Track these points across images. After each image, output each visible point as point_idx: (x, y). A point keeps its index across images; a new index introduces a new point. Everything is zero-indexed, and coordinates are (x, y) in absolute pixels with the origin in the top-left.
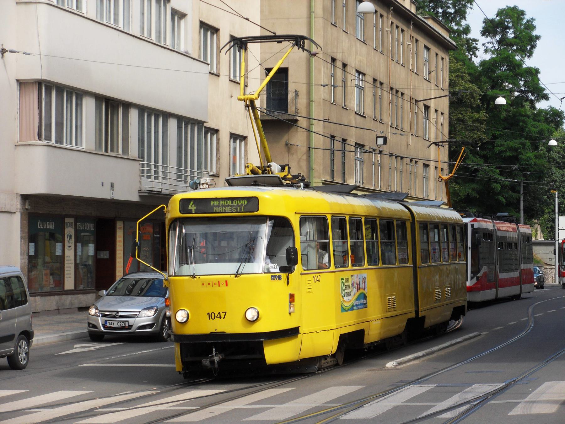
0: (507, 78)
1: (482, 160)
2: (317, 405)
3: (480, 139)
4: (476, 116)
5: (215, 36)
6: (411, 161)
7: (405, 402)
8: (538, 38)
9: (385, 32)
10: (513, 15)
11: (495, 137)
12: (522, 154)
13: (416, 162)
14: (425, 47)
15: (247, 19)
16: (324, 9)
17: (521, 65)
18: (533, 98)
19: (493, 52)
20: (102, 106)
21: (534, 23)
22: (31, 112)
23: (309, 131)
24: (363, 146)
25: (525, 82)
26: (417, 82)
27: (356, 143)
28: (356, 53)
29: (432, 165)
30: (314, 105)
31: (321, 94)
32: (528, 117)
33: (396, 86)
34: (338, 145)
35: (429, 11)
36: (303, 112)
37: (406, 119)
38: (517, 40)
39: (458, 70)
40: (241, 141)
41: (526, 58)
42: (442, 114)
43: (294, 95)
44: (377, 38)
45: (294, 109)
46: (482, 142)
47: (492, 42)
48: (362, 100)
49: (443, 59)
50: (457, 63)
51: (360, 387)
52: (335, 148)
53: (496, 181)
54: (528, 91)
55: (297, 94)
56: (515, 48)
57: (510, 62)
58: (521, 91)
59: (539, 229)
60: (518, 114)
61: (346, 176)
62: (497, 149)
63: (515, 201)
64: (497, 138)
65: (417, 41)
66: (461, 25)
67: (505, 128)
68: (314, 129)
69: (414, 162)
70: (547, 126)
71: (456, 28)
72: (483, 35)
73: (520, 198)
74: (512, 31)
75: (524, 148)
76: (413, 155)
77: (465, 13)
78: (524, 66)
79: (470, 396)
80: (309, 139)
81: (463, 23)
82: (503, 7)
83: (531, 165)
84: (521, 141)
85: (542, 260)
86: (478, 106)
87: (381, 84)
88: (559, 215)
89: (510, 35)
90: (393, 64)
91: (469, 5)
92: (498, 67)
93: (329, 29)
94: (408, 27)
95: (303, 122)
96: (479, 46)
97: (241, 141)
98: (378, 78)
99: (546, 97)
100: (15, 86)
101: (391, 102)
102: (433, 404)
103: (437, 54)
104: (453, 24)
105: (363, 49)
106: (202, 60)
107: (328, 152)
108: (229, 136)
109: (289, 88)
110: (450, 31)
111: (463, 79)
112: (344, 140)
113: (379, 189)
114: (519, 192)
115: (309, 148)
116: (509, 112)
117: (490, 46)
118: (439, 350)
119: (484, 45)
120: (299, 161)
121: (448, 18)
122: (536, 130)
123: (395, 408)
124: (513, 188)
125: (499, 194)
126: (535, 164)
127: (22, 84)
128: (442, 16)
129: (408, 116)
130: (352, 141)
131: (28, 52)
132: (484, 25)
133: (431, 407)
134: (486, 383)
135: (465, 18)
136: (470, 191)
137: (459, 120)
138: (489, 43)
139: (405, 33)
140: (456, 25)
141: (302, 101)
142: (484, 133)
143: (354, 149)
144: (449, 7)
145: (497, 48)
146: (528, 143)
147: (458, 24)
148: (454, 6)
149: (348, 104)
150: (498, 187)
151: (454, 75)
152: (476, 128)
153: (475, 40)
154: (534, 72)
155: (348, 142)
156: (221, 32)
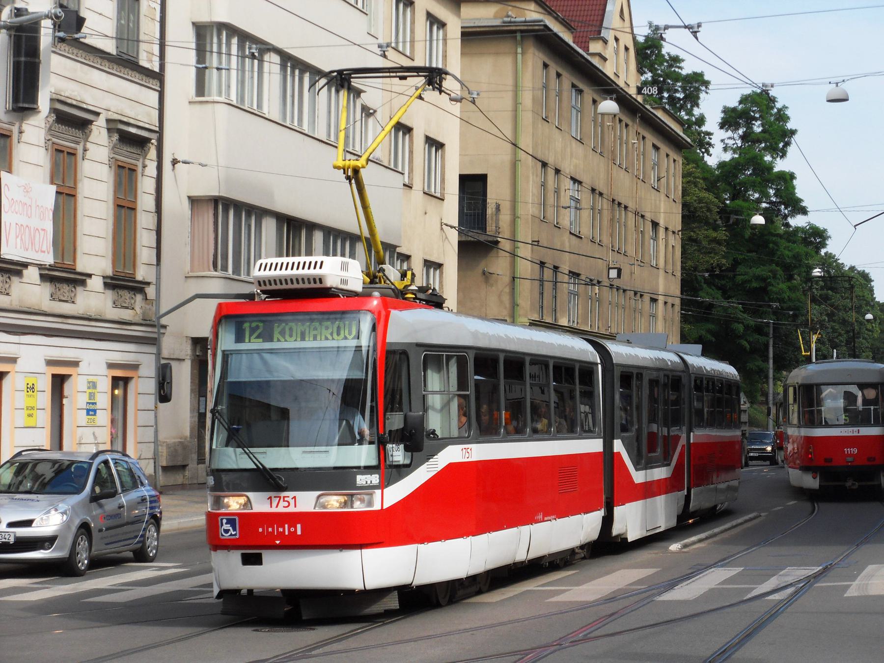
0: (754, 187)
1: (720, 292)
3: (718, 265)
4: (714, 235)
5: (407, 136)
6: (636, 293)
8: (793, 132)
13: (641, 296)
17: (772, 168)
18: (786, 212)
19: (735, 151)
20: (283, 227)
21: (788, 112)
22: (206, 236)
23: (513, 255)
24: (578, 275)
25: (777, 190)
27: (570, 272)
29: (661, 299)
30: (519, 221)
31: (529, 208)
32: (780, 236)
33: (618, 199)
34: (548, 274)
36: (505, 232)
37: (630, 240)
38: (767, 136)
40: (435, 269)
41: (778, 159)
47: (734, 137)
49: (674, 161)
50: (688, 164)
51: (650, 571)
52: (545, 278)
53: (738, 321)
54: (780, 203)
56: (763, 145)
57: (759, 164)
58: (771, 203)
61: (558, 315)
62: (739, 279)
64: (740, 264)
66: (693, 115)
67: (750, 251)
68: (520, 252)
69: (639, 295)
70: (805, 249)
71: (686, 118)
72: (721, 128)
74: (759, 122)
75: (775, 277)
77: (698, 98)
78: (776, 170)
79: (790, 579)
81: (696, 112)
87: (601, 194)
89: (757, 128)
90: (615, 168)
91: (703, 88)
94: (634, 121)
95: (505, 245)
98: (597, 188)
99: (804, 211)
100: (186, 204)
101: (612, 220)
103: (667, 155)
104: (683, 113)
106: (392, 167)
107: (537, 283)
108: (421, 263)
111: (696, 186)
112: (556, 268)
113: (596, 330)
114: (767, 335)
115: (514, 278)
117: (731, 142)
118: (722, 532)
119: (722, 141)
120: (499, 296)
121: (675, 104)
122: (790, 254)
123: (711, 590)
124: (760, 330)
125: (740, 337)
126: (790, 299)
127: (194, 201)
129: (632, 236)
130: (565, 268)
131: (204, 163)
132: (722, 115)
136: (703, 333)
138: (729, 138)
139: (630, 128)
140: (687, 114)
141: (505, 218)
142: (724, 257)
143: (566, 278)
144: (676, 91)
145: (739, 145)
146: (780, 271)
147: (690, 113)
149: (560, 221)
150: (741, 328)
153: (709, 134)
154: (788, 177)
155: (560, 270)
156: (415, 132)
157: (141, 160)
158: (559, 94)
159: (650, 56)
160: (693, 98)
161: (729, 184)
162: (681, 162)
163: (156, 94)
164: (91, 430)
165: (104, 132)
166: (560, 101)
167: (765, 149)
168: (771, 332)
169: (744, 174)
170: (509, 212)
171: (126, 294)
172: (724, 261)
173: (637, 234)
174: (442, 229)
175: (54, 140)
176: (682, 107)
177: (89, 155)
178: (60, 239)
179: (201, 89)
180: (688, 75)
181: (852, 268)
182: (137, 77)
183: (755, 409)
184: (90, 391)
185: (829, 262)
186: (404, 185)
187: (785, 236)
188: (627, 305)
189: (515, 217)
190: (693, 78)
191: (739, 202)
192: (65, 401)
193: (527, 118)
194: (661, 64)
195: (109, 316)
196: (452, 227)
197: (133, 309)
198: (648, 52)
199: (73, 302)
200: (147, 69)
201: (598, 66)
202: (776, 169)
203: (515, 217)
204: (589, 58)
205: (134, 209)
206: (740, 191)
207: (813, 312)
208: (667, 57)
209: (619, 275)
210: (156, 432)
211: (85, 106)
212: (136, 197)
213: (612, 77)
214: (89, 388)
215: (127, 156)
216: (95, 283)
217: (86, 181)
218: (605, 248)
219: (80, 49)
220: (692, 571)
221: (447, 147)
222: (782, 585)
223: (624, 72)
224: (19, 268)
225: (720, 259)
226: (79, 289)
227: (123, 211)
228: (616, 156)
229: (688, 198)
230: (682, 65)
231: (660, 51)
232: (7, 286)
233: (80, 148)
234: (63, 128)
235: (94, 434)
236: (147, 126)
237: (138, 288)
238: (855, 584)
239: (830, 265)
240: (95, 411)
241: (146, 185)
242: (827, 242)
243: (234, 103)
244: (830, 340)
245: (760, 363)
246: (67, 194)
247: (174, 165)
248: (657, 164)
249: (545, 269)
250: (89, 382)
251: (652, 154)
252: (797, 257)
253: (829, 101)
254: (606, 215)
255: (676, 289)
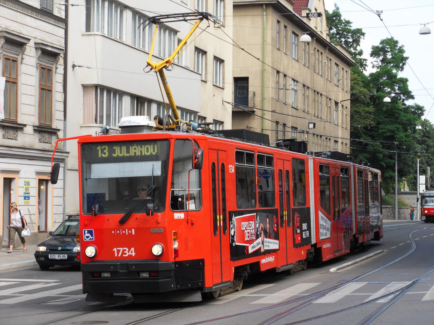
0: (387, 85)
2: (295, 295)
4: (367, 109)
5: (204, 56)
6: (327, 138)
7: (351, 293)
8: (407, 58)
9: (310, 54)
10: (391, 43)
11: (379, 123)
12: (397, 134)
13: (330, 139)
14: (336, 64)
15: (243, 49)
16: (272, 39)
18: (404, 98)
19: (378, 68)
21: (404, 48)
24: (296, 128)
25: (399, 87)
26: (330, 86)
27: (292, 127)
28: (292, 67)
29: (340, 141)
32: (401, 110)
34: (280, 127)
35: (336, 40)
36: (258, 105)
39: (355, 79)
40: (220, 125)
42: (346, 108)
43: (252, 95)
44: (305, 58)
45: (252, 104)
46: (371, 127)
47: (377, 61)
48: (296, 98)
49: (346, 72)
50: (354, 74)
52: (279, 130)
54: (401, 93)
55: (254, 94)
56: (392, 65)
57: (389, 74)
58: (396, 93)
59: (406, 184)
60: (394, 108)
62: (380, 131)
63: (393, 165)
65: (330, 60)
66: (357, 50)
67: (386, 117)
69: (328, 139)
70: (413, 116)
71: (353, 51)
72: (371, 56)
73: (395, 163)
74: (390, 53)
75: (398, 130)
76: (328, 134)
77: (359, 41)
78: (398, 77)
79: (393, 289)
80: (262, 123)
81: (359, 48)
82: (384, 38)
83: (402, 141)
84: (396, 126)
85: (409, 204)
86: (368, 103)
87: (308, 88)
88: (419, 175)
91: (362, 36)
92: (381, 77)
93: (275, 52)
94: (325, 52)
95: (258, 113)
96: (368, 63)
97: (220, 125)
99: (412, 97)
100: (81, 88)
101: (314, 100)
102: (352, 294)
103: (343, 69)
104: (352, 49)
105: (296, 65)
106: (196, 71)
109: (249, 90)
110: (350, 53)
111: (358, 85)
112: (284, 125)
114: (394, 159)
116: (388, 107)
117: (376, 63)
118: (360, 261)
119: (372, 63)
122: (406, 119)
123: (347, 296)
124: (391, 157)
125: (381, 160)
126: (406, 141)
127: (85, 87)
128: (345, 44)
129: (325, 109)
130: (289, 125)
131: (89, 67)
132: (372, 50)
133: (368, 296)
134: (400, 281)
135: (359, 45)
137: (356, 111)
139: (323, 54)
140: (354, 49)
141: (258, 99)
143: (290, 130)
144: (349, 38)
145: (380, 65)
147: (355, 49)
148: (352, 37)
149: (286, 101)
150: (381, 155)
151: (352, 82)
152: (367, 118)
153: (365, 60)
154: (405, 81)
155: (287, 125)
156: (208, 54)
157: (55, 65)
158: (286, 37)
159: (335, 21)
160: (357, 42)
161: (375, 84)
162: (350, 72)
163: (63, 31)
164: (27, 207)
165: (33, 50)
166: (286, 40)
167: (393, 67)
168: (397, 158)
169: (382, 79)
170: (260, 96)
171: (47, 136)
172: (372, 123)
173: (327, 108)
174: (223, 104)
175: (5, 53)
176: (351, 46)
177: (24, 61)
178: (8, 106)
179: (88, 28)
180: (354, 30)
181: (419, 110)
182: (52, 21)
183: (389, 197)
184: (26, 186)
185: (425, 124)
186: (201, 81)
187: (403, 110)
188: (322, 144)
189: (263, 99)
190: (357, 31)
191: (380, 93)
192: (12, 192)
193: (269, 48)
194: (341, 25)
195: (36, 147)
196: (228, 103)
197: (50, 143)
198: (333, 19)
199: (16, 140)
200: (58, 17)
201: (306, 23)
202: (398, 77)
203: (263, 99)
204: (301, 18)
205: (51, 91)
206: (380, 88)
207: (418, 148)
208: (344, 21)
209: (314, 127)
210: (64, 208)
211: (22, 36)
212: (52, 84)
213: (314, 28)
214: (25, 185)
215: (46, 63)
216: (29, 130)
217: (23, 75)
218: (310, 115)
219: (19, 5)
220: (338, 284)
221: (225, 62)
222: (387, 293)
223: (319, 26)
224: (22, 127)
225: (370, 122)
226: (19, 133)
227: (44, 91)
228: (316, 69)
229: (354, 91)
230: (351, 25)
231: (340, 18)
232: (50, 139)
233: (19, 58)
234: (9, 47)
235: (28, 209)
236: (58, 47)
237: (54, 132)
238: (428, 292)
239: (426, 125)
240: (29, 198)
241: (58, 78)
242: (424, 113)
243: (106, 35)
244: (426, 162)
245: (391, 173)
246: (12, 82)
247: (73, 68)
248: (337, 73)
249: (279, 125)
250: (25, 182)
251: (335, 68)
252: (409, 120)
253: (420, 34)
254: (300, 93)
255: (347, 135)
